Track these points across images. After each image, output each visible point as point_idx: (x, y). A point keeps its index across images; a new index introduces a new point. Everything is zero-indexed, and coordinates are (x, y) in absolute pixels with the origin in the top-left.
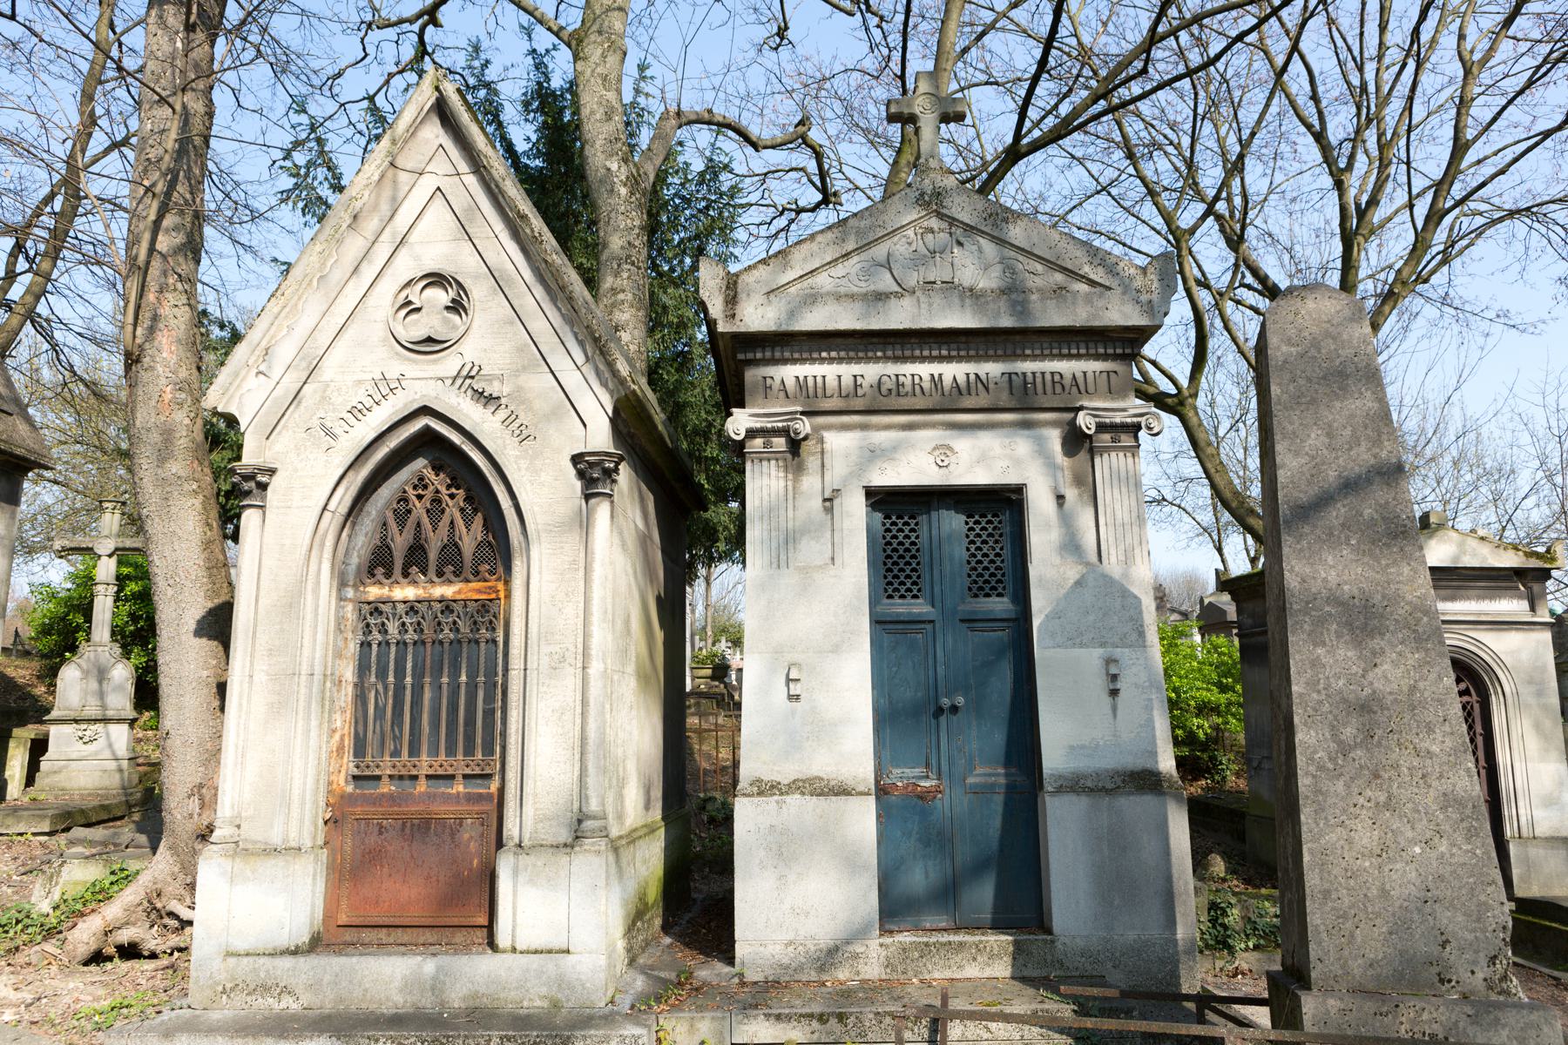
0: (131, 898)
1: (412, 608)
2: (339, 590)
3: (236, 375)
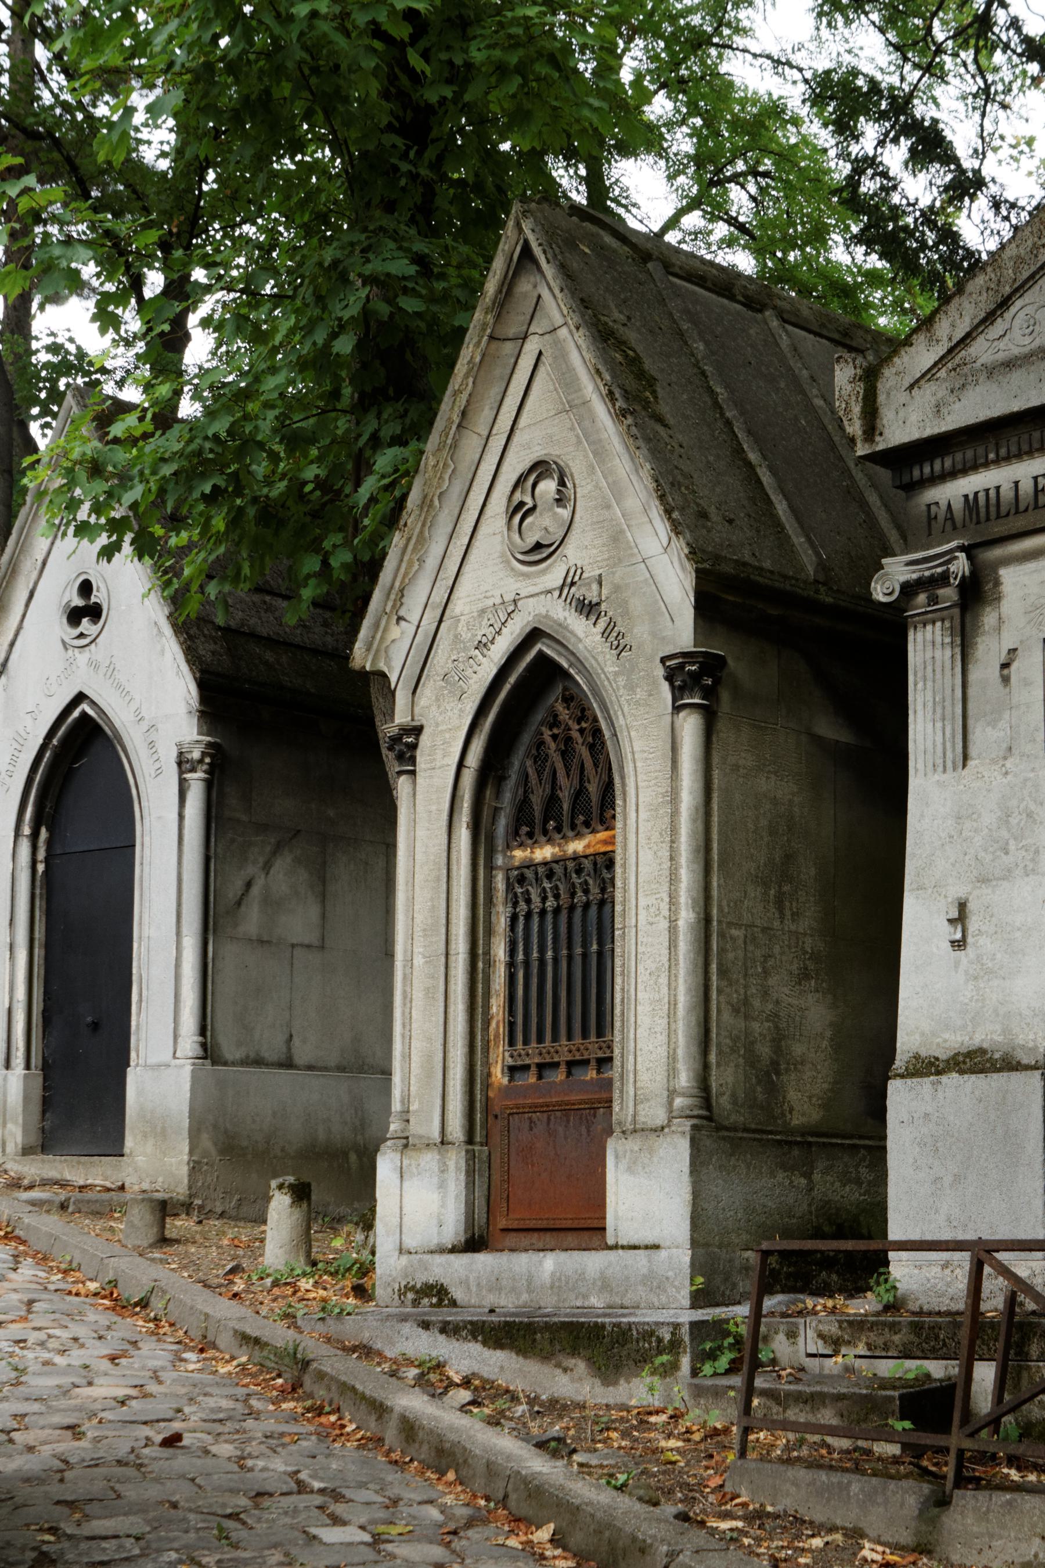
3: (376, 626)
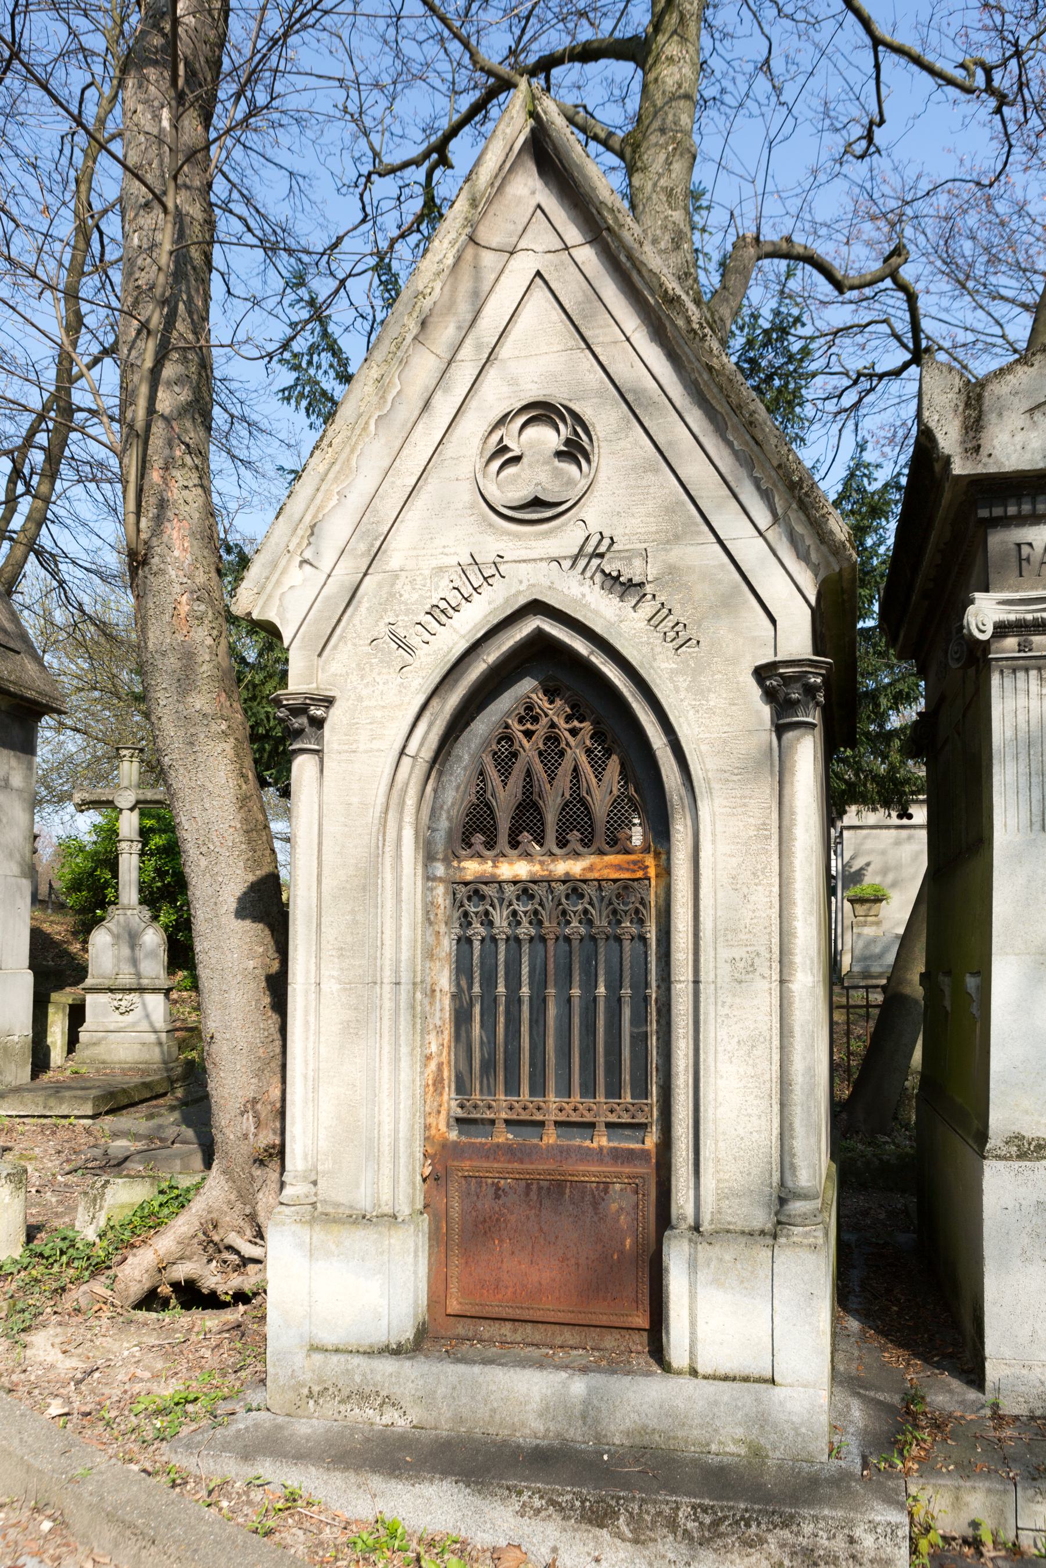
0: (184, 1229)
1: (525, 891)
2: (425, 866)
3: (274, 565)
